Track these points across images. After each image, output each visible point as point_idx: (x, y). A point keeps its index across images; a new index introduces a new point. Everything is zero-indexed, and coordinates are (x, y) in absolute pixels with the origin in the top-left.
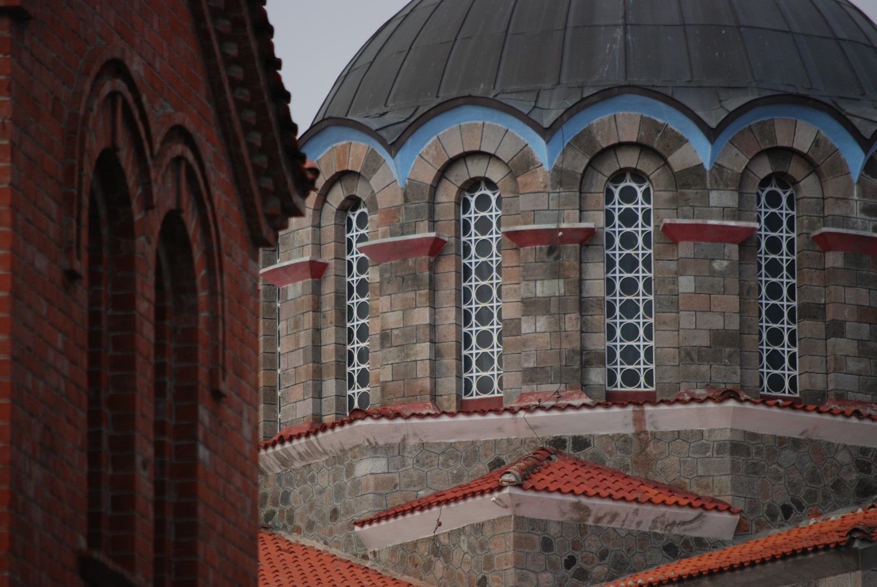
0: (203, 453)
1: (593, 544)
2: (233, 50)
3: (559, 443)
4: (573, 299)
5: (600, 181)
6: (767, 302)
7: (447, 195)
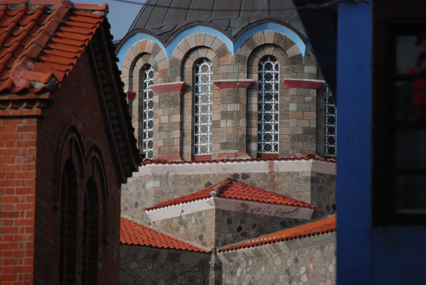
0: (100, 265)
1: (250, 221)
2: (114, 114)
3: (236, 176)
4: (244, 113)
5: (256, 61)
6: (329, 115)
7: (189, 65)
